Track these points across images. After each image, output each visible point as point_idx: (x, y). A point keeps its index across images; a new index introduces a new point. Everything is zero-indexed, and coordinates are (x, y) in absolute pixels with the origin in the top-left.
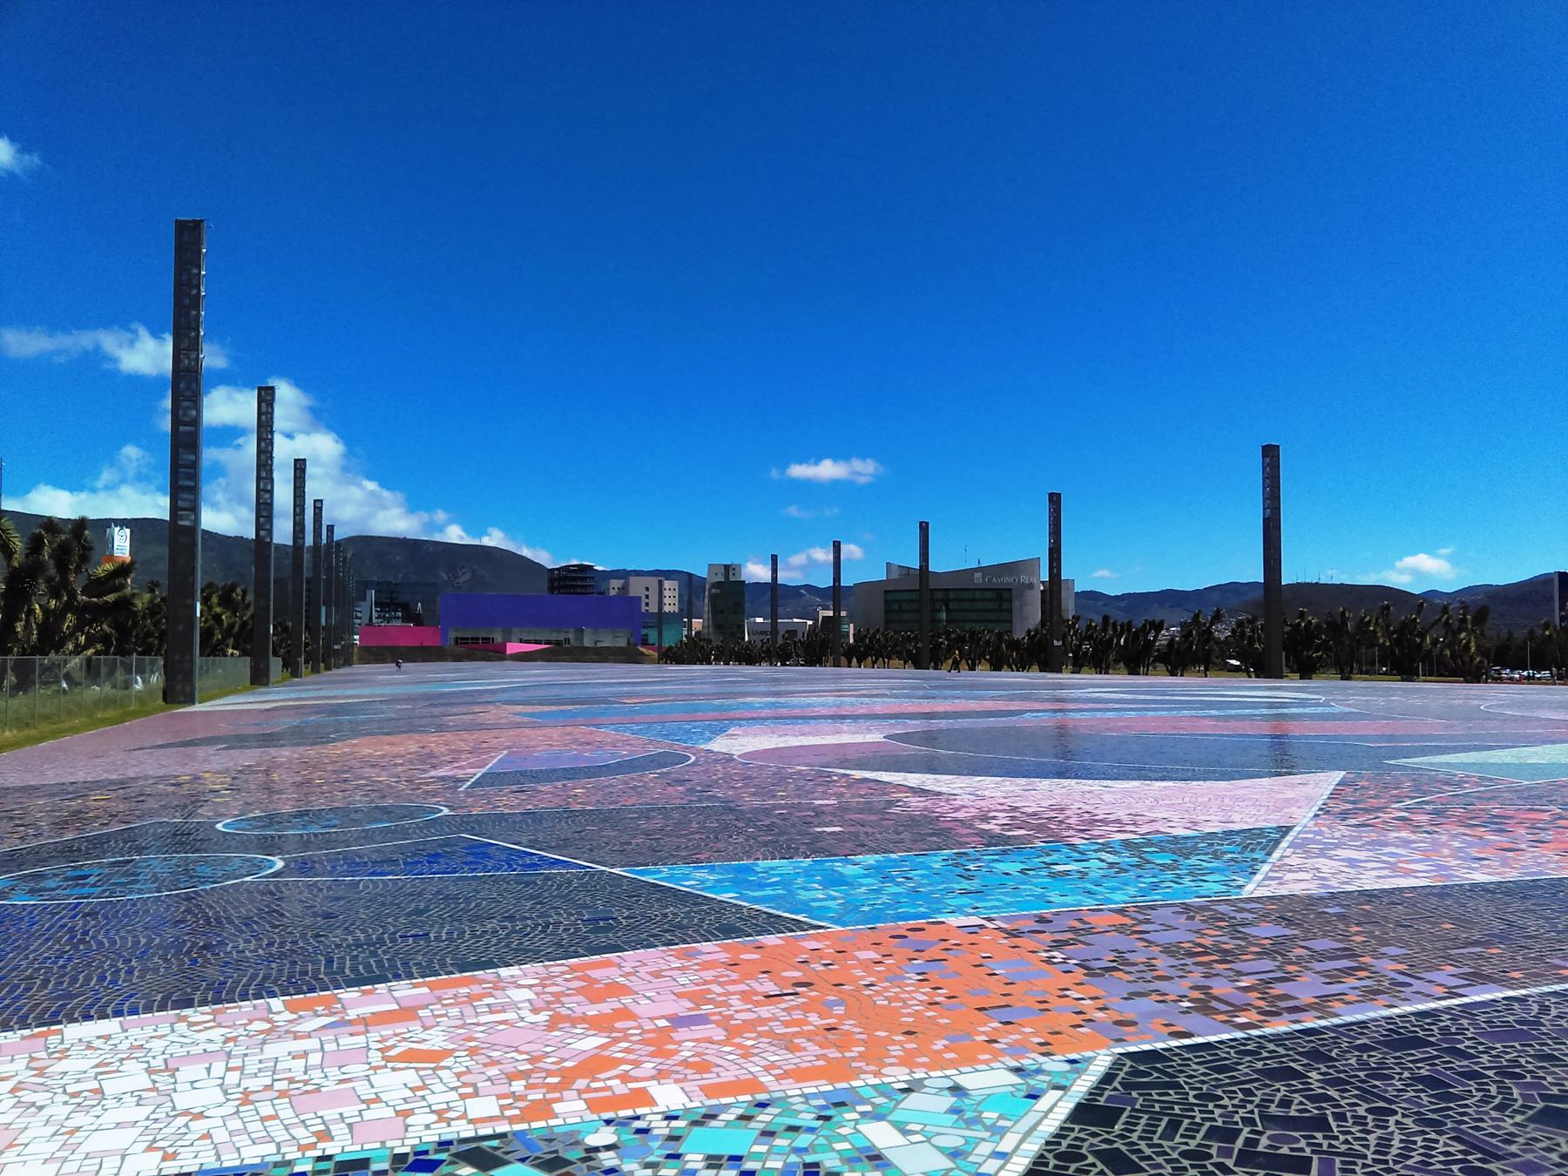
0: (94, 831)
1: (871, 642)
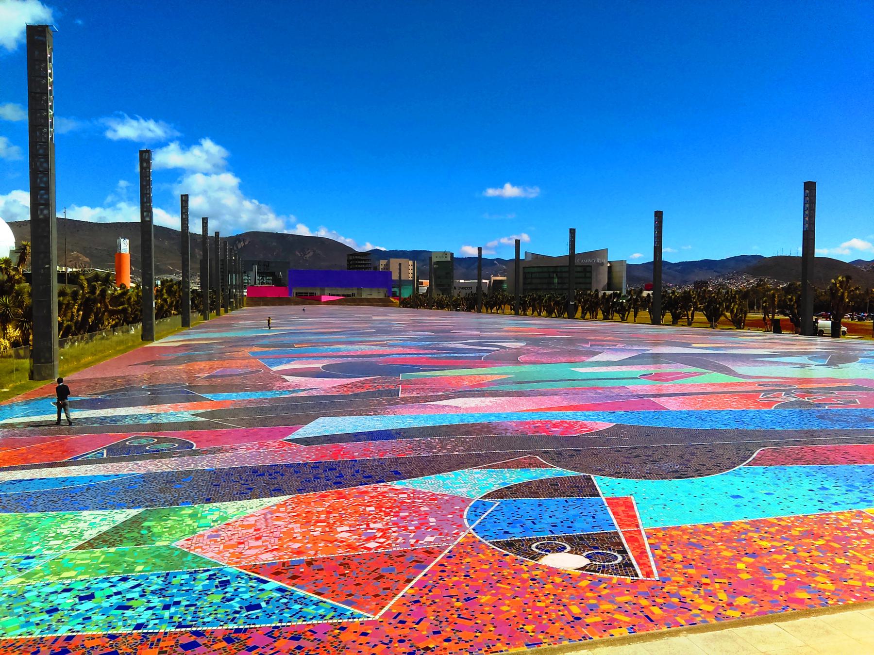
0: (119, 388)
1: (496, 299)
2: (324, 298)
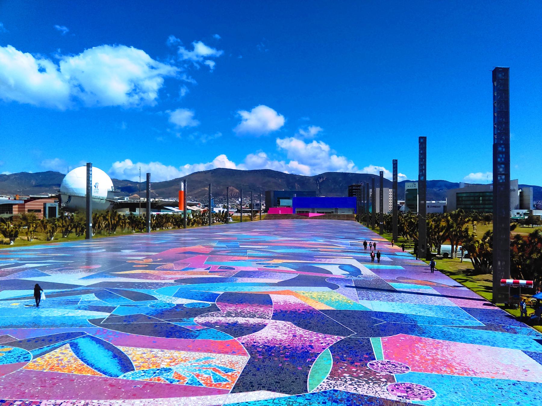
2: (311, 215)
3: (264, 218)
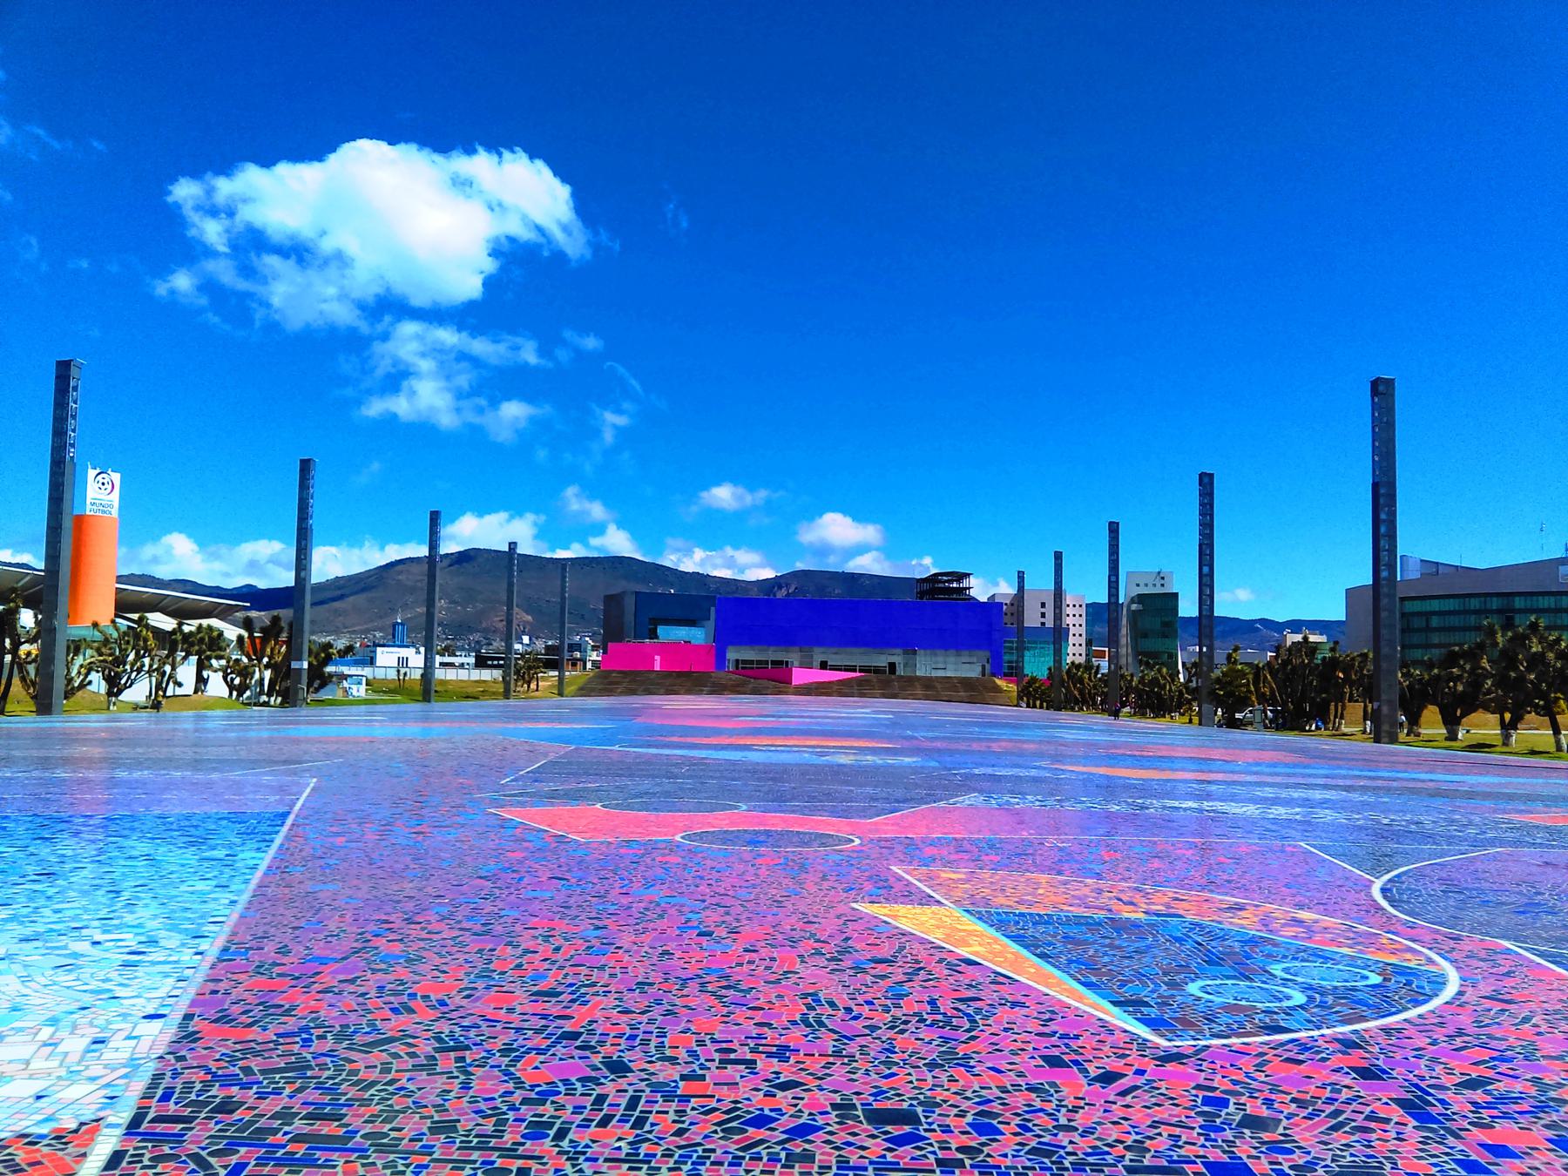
2: (800, 676)
3: (581, 689)
